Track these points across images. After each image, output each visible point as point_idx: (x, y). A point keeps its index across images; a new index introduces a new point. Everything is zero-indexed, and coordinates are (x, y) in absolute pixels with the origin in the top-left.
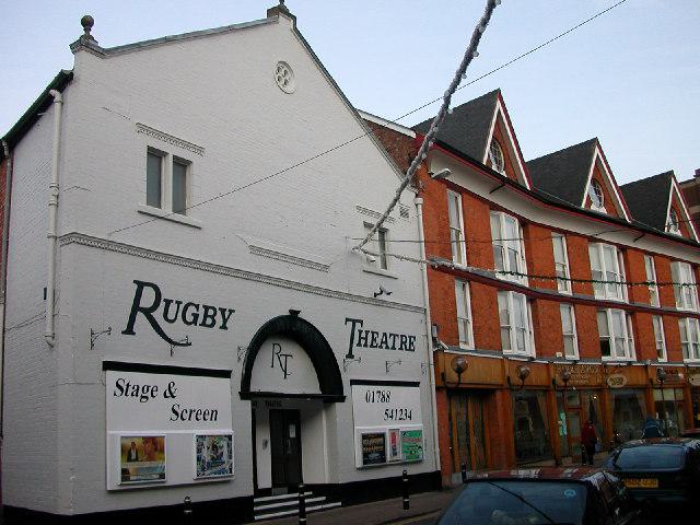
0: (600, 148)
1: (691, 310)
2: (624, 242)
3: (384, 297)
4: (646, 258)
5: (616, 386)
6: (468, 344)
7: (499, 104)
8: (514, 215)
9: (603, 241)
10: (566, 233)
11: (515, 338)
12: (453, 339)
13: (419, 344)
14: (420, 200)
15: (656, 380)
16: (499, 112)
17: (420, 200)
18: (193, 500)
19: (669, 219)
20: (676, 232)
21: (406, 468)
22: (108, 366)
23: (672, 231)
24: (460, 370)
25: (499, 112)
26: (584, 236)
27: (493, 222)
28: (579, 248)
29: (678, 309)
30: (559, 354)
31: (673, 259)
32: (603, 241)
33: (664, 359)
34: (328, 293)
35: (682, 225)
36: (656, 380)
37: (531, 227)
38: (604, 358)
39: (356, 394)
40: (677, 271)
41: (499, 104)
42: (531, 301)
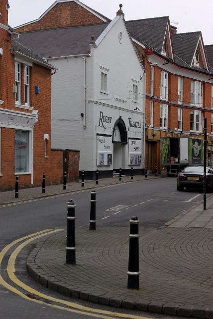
0: (201, 37)
2: (206, 80)
3: (137, 110)
7: (200, 38)
8: (200, 81)
9: (197, 80)
13: (142, 125)
14: (146, 74)
16: (200, 41)
17: (146, 74)
18: (99, 170)
19: (194, 58)
20: (196, 65)
22: (98, 134)
23: (195, 64)
24: (154, 136)
25: (200, 41)
28: (187, 81)
29: (192, 105)
30: (176, 129)
32: (197, 80)
34: (125, 110)
37: (206, 85)
38: (191, 131)
39: (130, 141)
41: (200, 38)
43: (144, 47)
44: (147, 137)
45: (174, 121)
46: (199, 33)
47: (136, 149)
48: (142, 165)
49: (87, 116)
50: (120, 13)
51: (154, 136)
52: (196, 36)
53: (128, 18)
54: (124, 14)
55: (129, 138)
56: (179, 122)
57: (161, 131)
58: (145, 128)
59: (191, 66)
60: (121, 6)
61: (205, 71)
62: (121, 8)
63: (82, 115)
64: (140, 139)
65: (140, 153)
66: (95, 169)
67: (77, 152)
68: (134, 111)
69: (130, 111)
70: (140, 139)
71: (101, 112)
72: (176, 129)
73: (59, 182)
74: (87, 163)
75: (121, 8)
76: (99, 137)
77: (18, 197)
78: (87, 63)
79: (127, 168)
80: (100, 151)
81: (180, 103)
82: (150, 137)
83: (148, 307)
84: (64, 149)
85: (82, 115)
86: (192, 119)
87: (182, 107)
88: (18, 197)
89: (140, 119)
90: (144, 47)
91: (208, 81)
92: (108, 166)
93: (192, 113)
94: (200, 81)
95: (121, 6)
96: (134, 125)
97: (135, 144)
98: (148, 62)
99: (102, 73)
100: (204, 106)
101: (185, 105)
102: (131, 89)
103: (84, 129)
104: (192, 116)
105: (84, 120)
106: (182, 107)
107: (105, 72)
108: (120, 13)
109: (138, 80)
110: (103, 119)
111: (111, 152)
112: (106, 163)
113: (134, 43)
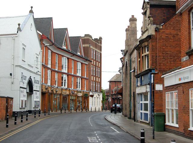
1: (65, 72)
4: (56, 55)
5: (64, 94)
6: (49, 84)
7: (67, 32)
8: (80, 62)
10: (58, 54)
11: (133, 89)
12: (46, 82)
15: (71, 94)
18: (36, 110)
20: (65, 48)
21: (35, 108)
22: (21, 87)
23: (64, 47)
26: (61, 55)
27: (62, 58)
29: (77, 75)
30: (54, 85)
31: (63, 56)
33: (73, 88)
35: (67, 46)
36: (71, 94)
38: (62, 87)
39: (34, 92)
40: (78, 64)
41: (67, 32)
42: (68, 76)
43: (41, 34)
44: (42, 90)
45: (53, 80)
46: (66, 29)
47: (37, 98)
48: (39, 108)
49: (14, 75)
50: (31, 12)
51: (56, 92)
52: (64, 31)
53: (36, 17)
54: (33, 13)
55: (34, 90)
56: (56, 81)
57: (62, 89)
58: (41, 84)
59: (62, 48)
60: (32, 7)
61: (82, 57)
62: (32, 9)
63: (11, 74)
64: (39, 91)
65: (38, 100)
66: (19, 110)
67: (12, 98)
68: (36, 73)
69: (34, 73)
70: (39, 91)
71: (22, 73)
72: (54, 85)
73: (4, 119)
74: (16, 108)
75: (32, 9)
76: (21, 89)
77: (16, 124)
78: (15, 40)
79: (33, 109)
80: (21, 99)
81: (57, 70)
82: (44, 90)
83: (187, 127)
84: (6, 96)
85: (11, 74)
86: (62, 80)
87: (58, 72)
88: (16, 124)
89: (38, 78)
90: (41, 34)
91: (71, 58)
92: (24, 108)
93: (62, 76)
94: (80, 62)
95: (32, 7)
96: (37, 82)
97: (36, 94)
98: (43, 43)
99: (23, 48)
100: (68, 72)
101: (59, 71)
102: (35, 59)
103: (12, 83)
104: (62, 77)
105: (12, 78)
106: (58, 72)
107: (24, 47)
108: (31, 12)
109: (39, 54)
110: (23, 77)
111: (26, 99)
112: (24, 107)
113: (37, 33)
